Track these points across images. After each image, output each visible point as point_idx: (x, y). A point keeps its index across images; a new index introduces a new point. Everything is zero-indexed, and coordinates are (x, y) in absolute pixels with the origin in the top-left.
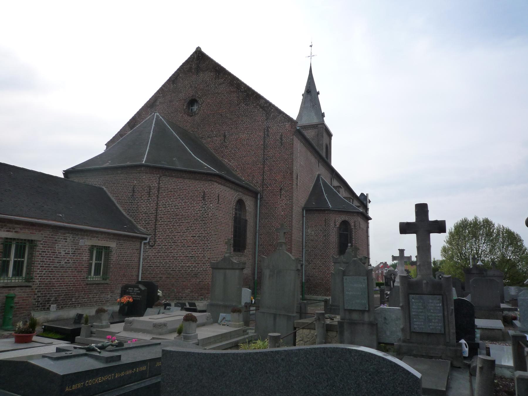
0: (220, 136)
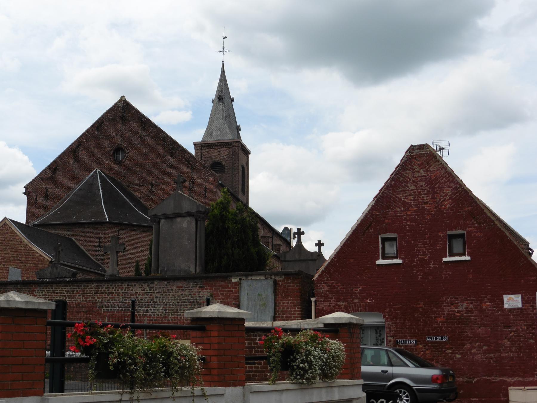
0: (147, 185)
